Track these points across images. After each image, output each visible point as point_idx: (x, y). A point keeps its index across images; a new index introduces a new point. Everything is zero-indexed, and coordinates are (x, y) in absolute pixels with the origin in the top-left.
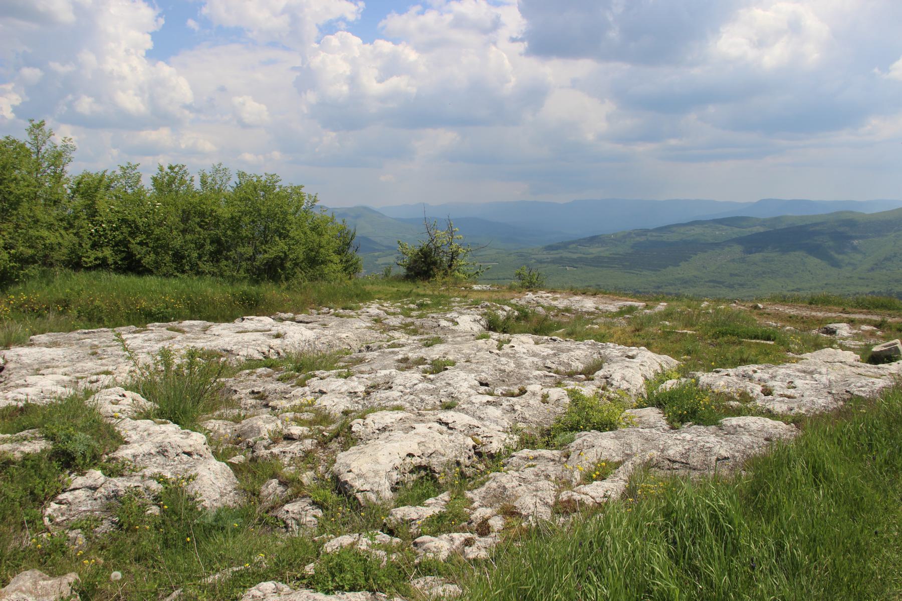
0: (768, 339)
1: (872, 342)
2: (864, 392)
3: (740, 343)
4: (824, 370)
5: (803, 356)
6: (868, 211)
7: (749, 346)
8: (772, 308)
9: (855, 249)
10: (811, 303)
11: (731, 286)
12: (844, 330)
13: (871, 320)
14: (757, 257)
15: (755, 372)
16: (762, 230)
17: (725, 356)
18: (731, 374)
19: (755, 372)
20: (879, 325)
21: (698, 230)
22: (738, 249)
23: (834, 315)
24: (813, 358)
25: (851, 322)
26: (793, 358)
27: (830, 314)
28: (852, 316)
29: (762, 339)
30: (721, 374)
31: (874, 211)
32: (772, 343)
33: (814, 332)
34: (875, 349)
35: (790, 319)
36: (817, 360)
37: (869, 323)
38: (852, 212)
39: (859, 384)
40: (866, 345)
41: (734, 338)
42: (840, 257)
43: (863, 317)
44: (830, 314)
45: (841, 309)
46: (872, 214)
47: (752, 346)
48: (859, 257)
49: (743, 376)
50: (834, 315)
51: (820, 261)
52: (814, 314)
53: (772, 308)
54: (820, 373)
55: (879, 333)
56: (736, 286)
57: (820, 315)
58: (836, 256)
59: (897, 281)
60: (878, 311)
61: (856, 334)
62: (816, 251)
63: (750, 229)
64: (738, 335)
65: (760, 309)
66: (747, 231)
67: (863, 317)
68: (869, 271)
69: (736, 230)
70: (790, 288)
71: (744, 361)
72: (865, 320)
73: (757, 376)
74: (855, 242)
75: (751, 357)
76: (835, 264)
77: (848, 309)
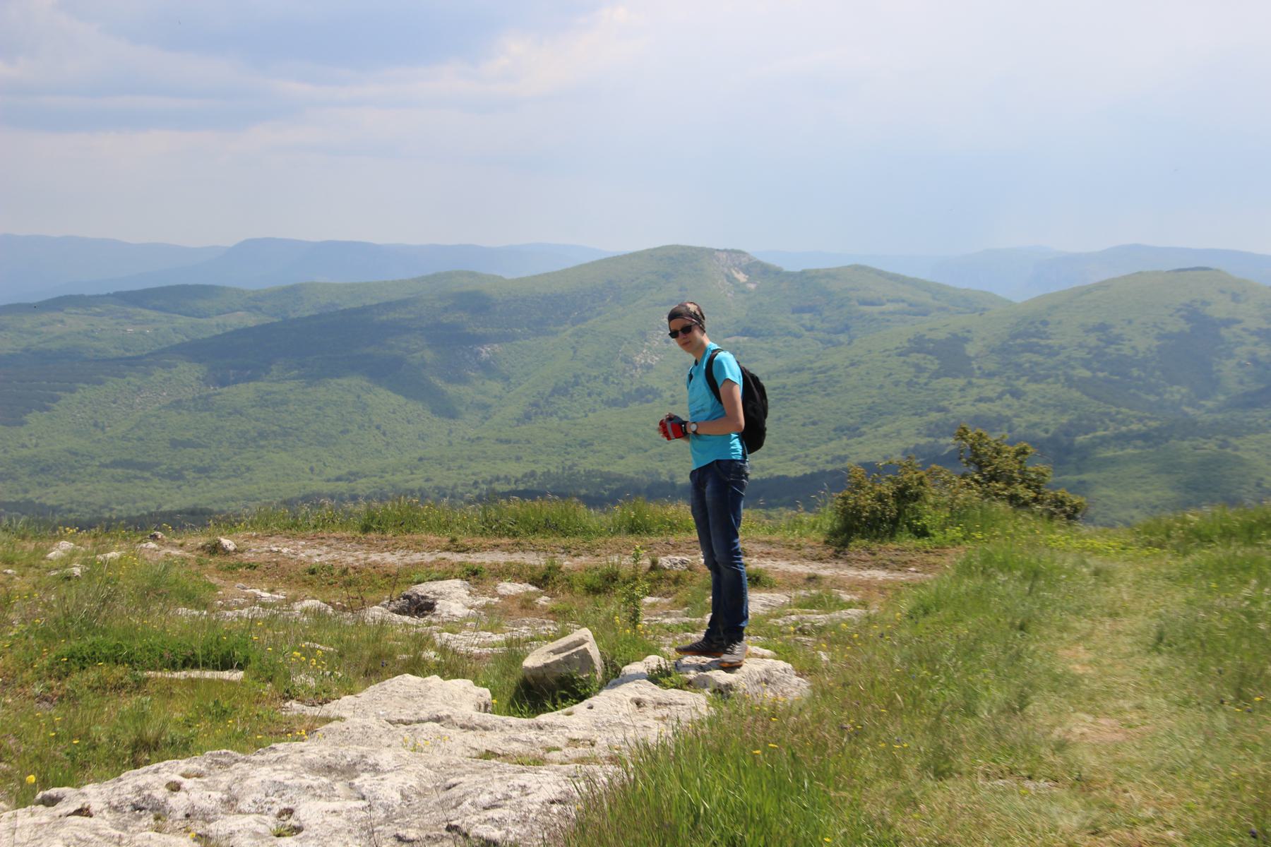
0: (226, 665)
1: (524, 632)
2: (499, 823)
3: (139, 685)
4: (385, 758)
5: (331, 709)
6: (512, 272)
7: (167, 692)
8: (261, 548)
9: (488, 369)
10: (366, 529)
11: (176, 476)
12: (454, 598)
13: (521, 567)
14: (243, 393)
15: (175, 787)
16: (251, 320)
17: (85, 736)
18: (96, 805)
19: (175, 787)
20: (543, 580)
21: (73, 323)
22: (189, 374)
23: (428, 558)
24: (363, 710)
25: (473, 575)
26: (301, 718)
27: (417, 557)
28: (475, 559)
29: (206, 665)
30: (61, 809)
31: (526, 273)
32: (238, 675)
33: (376, 612)
34: (533, 661)
35: (313, 576)
36: (371, 721)
37: (516, 574)
38: (472, 275)
39: (485, 799)
40: (509, 643)
41: (119, 671)
42: (452, 390)
43: (500, 558)
44: (417, 557)
45: (445, 541)
46: (520, 280)
47: (167, 702)
48: (495, 387)
49: (136, 807)
50: (428, 558)
51: (402, 399)
52: (375, 557)
53: (261, 548)
54: (375, 769)
55: (543, 600)
56: (190, 475)
57: (391, 559)
58: (440, 383)
59: (584, 444)
60: (539, 540)
61: (486, 607)
62: (390, 373)
63: (219, 320)
64: (130, 660)
65: (226, 552)
66: (213, 325)
67: (500, 558)
68: (520, 421)
69: (182, 321)
70: (331, 472)
71: (144, 750)
72: (509, 565)
73: (178, 802)
74: (485, 352)
75: (172, 731)
76: (447, 410)
77: (463, 540)
